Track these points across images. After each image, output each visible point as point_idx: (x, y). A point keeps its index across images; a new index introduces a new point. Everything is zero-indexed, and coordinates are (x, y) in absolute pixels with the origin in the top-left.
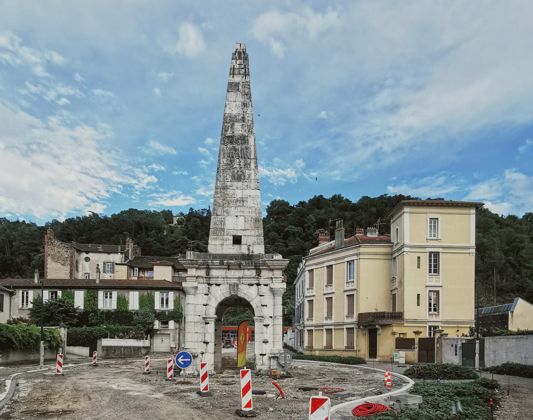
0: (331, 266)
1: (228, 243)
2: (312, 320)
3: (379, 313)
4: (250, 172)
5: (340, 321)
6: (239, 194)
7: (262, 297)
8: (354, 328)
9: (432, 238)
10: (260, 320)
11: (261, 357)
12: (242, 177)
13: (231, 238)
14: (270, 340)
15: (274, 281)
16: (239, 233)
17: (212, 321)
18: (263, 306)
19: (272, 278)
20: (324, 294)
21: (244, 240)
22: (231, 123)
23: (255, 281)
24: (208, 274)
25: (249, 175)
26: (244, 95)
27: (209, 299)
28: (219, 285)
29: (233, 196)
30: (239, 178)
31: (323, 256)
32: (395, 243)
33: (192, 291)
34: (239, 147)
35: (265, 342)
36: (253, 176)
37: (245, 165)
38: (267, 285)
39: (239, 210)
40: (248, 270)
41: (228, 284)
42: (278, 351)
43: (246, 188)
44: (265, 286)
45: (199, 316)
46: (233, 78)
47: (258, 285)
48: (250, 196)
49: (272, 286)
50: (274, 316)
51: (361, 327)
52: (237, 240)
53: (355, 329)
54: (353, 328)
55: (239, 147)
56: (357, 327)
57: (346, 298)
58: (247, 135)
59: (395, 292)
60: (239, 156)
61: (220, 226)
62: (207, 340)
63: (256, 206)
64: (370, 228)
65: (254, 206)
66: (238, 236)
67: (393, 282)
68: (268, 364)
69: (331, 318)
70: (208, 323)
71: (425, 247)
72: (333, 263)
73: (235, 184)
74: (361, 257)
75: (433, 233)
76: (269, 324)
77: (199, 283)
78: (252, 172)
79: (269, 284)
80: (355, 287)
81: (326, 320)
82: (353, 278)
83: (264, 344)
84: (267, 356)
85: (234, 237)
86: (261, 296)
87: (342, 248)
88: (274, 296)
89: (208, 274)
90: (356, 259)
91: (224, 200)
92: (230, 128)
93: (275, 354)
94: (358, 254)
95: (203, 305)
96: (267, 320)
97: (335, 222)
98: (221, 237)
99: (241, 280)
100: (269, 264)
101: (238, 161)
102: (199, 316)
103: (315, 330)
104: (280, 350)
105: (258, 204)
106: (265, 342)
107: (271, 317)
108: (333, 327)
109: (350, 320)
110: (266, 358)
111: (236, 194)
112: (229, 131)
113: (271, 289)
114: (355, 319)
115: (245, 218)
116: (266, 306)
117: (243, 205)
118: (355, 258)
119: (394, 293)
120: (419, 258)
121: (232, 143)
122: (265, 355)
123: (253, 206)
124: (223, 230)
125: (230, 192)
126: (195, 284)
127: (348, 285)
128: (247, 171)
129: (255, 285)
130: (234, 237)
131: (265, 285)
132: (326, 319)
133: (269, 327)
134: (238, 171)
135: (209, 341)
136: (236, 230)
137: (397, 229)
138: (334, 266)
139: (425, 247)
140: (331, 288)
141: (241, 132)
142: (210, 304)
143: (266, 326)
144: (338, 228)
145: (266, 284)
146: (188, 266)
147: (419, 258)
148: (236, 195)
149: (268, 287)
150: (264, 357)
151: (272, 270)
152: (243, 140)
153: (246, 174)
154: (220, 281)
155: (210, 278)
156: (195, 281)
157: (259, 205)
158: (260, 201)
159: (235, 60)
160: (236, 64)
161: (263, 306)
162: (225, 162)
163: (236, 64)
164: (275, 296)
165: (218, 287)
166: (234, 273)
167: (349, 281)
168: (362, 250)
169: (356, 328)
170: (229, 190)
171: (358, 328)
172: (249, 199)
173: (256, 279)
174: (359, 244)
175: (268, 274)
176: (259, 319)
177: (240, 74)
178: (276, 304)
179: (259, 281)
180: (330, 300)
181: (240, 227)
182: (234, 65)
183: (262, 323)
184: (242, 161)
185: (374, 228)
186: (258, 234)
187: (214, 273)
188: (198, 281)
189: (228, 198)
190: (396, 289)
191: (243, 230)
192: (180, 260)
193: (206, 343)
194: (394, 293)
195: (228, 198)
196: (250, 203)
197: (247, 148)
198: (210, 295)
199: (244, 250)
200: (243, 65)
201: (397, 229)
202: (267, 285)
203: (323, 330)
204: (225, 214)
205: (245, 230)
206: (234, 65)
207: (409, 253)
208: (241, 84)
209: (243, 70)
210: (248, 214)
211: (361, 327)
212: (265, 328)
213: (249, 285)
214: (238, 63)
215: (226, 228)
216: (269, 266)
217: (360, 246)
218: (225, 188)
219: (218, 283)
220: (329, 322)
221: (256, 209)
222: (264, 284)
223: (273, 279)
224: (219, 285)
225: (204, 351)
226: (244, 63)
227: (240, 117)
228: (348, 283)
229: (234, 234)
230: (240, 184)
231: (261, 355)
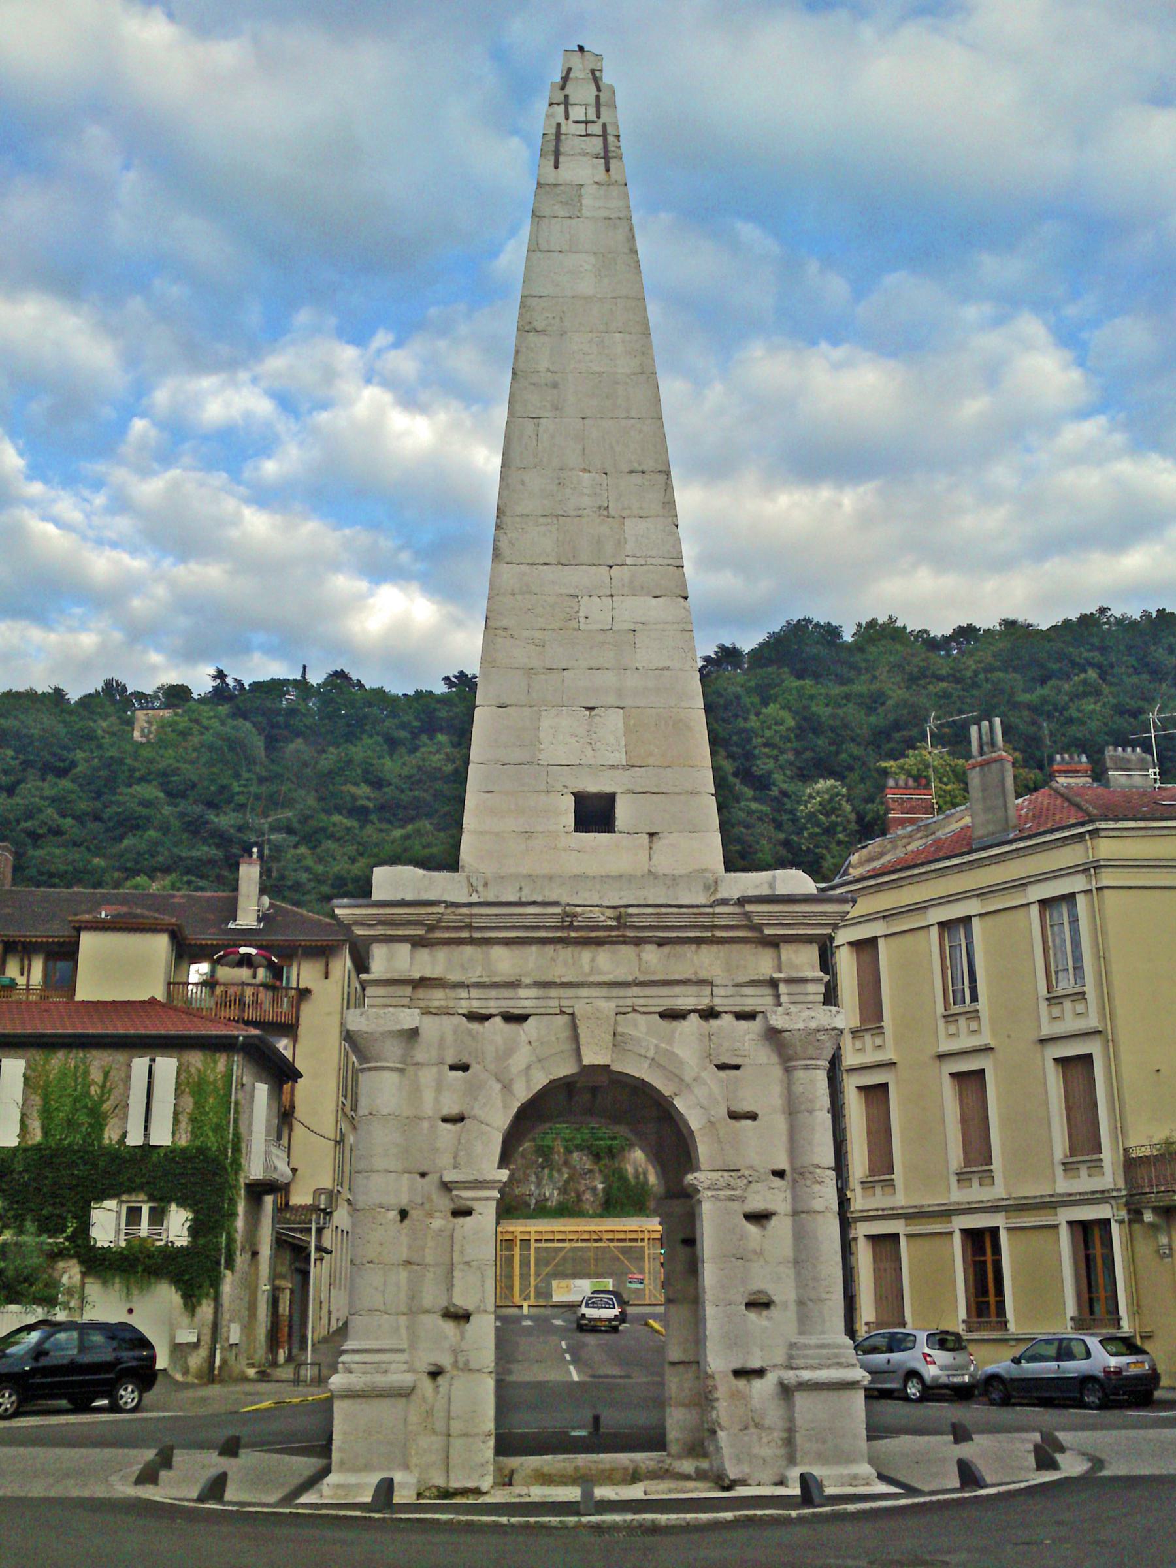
0: (872, 942)
2: (891, 1184)
5: (930, 1200)
8: (1109, 1220)
14: (784, 1292)
15: (784, 999)
17: (487, 1199)
18: (734, 1116)
19: (773, 984)
20: (941, 1057)
21: (623, 812)
27: (473, 1091)
28: (521, 1018)
31: (881, 896)
33: (392, 1051)
35: (760, 1304)
38: (750, 1016)
41: (562, 1013)
44: (743, 1022)
45: (423, 1175)
46: (556, 167)
49: (777, 1020)
50: (794, 1169)
51: (1148, 1217)
53: (1115, 1227)
54: (1107, 1222)
56: (1123, 1214)
57: (948, 1090)
62: (461, 1301)
64: (1129, 749)
68: (781, 1424)
69: (987, 1177)
70: (468, 1212)
72: (971, 907)
74: (1107, 878)
76: (771, 1207)
77: (426, 1012)
79: (758, 1009)
80: (1093, 1022)
81: (1070, 1174)
82: (974, 998)
83: (752, 1316)
84: (771, 1378)
85: (581, 799)
86: (722, 1067)
87: (1011, 842)
88: (788, 1070)
90: (1085, 892)
94: (1091, 868)
95: (445, 1120)
97: (964, 727)
102: (423, 1175)
103: (907, 1236)
106: (760, 1304)
107: (780, 1174)
108: (997, 1220)
109: (1085, 1183)
110: (763, 1389)
111: (581, 614)
113: (773, 1035)
114: (1110, 1177)
115: (626, 718)
118: (1077, 884)
122: (760, 1373)
123: (661, 666)
126: (409, 1018)
127: (1056, 1011)
129: (694, 1017)
130: (581, 799)
131: (740, 1016)
132: (963, 1177)
133: (774, 1221)
135: (471, 1308)
138: (881, 942)
142: (477, 1111)
144: (981, 753)
145: (747, 1009)
146: (379, 931)
148: (582, 620)
149: (756, 1026)
150: (758, 1384)
151: (774, 943)
154: (525, 999)
156: (406, 1001)
159: (562, 107)
160: (567, 118)
161: (734, 1116)
163: (567, 118)
164: (795, 1068)
165: (513, 1027)
166: (593, 960)
167: (955, 1009)
168: (1106, 848)
169: (1121, 1222)
171: (1130, 1222)
174: (1091, 821)
178: (803, 1107)
180: (970, 1082)
182: (559, 125)
185: (1133, 751)
188: (422, 1004)
192: (338, 907)
193: (461, 1317)
200: (593, 122)
202: (750, 1016)
203: (1056, 1226)
206: (559, 125)
211: (1148, 1217)
212: (752, 1229)
213: (663, 1015)
216: (758, 928)
217: (1097, 830)
219: (517, 1009)
220: (977, 1193)
222: (737, 1009)
223: (783, 988)
224: (521, 1018)
225: (446, 1361)
226: (599, 117)
228: (1054, 1000)
231: (739, 1373)
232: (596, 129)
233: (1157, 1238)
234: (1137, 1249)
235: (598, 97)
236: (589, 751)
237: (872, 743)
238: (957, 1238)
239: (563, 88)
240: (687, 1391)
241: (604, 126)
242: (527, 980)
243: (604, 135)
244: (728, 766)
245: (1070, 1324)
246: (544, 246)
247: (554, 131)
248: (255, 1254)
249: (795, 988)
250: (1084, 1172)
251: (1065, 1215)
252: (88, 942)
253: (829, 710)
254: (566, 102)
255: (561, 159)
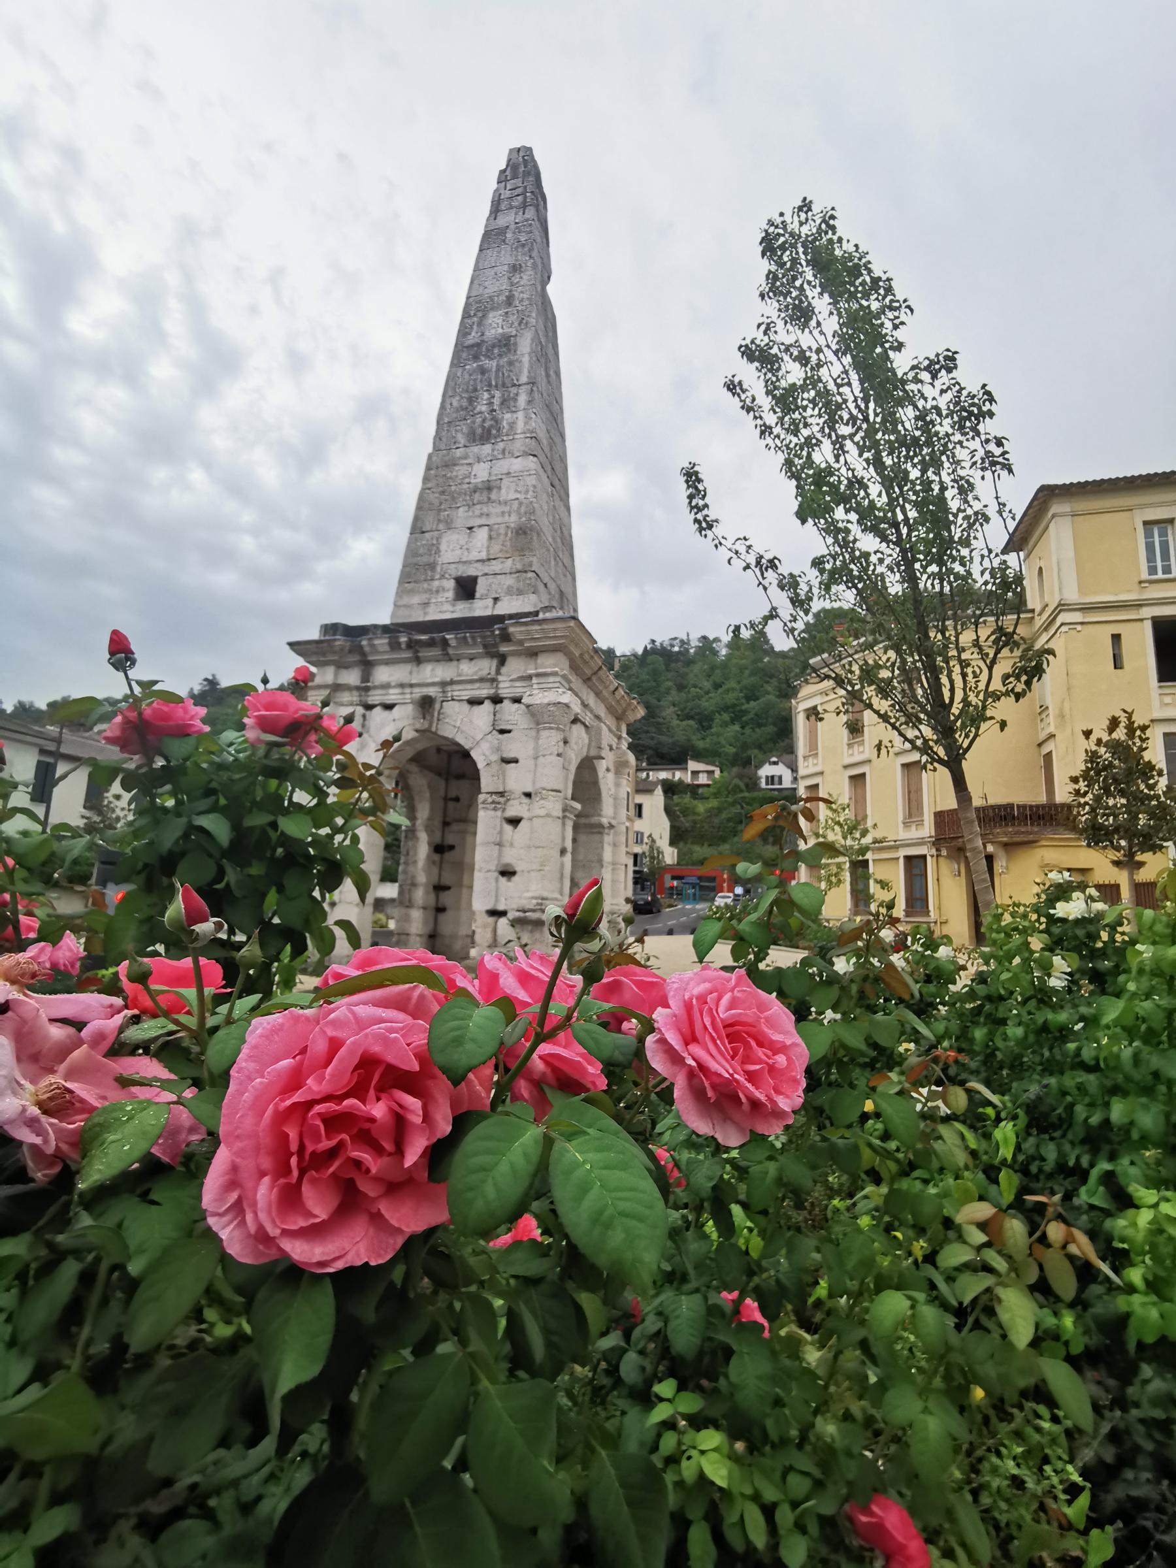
1: (440, 600)
3: (993, 807)
4: (515, 415)
6: (481, 473)
7: (506, 735)
9: (1160, 575)
10: (493, 802)
11: (491, 920)
12: (494, 432)
13: (450, 584)
16: (471, 571)
20: (846, 767)
21: (480, 589)
22: (480, 314)
23: (484, 691)
24: (366, 677)
25: (512, 425)
26: (516, 248)
29: (467, 480)
30: (486, 435)
32: (1038, 610)
34: (492, 364)
35: (507, 873)
36: (520, 426)
37: (502, 403)
39: (477, 512)
40: (471, 659)
42: (534, 901)
43: (500, 456)
47: (497, 700)
48: (509, 473)
52: (466, 588)
53: (929, 858)
54: (924, 857)
55: (492, 364)
56: (934, 852)
58: (514, 333)
59: (1049, 747)
60: (490, 385)
61: (425, 559)
63: (521, 496)
65: (518, 496)
66: (469, 577)
67: (1042, 720)
71: (1138, 605)
73: (475, 449)
75: (1159, 564)
78: (520, 415)
83: (503, 880)
86: (502, 732)
89: (366, 677)
91: (443, 493)
92: (475, 327)
93: (525, 912)
96: (515, 802)
98: (426, 586)
99: (449, 688)
100: (519, 637)
101: (486, 395)
104: (543, 899)
105: (527, 492)
106: (507, 873)
109: (914, 833)
112: (473, 334)
114: (928, 829)
115: (490, 530)
116: (516, 761)
117: (489, 499)
119: (1046, 749)
120: (1116, 638)
121: (476, 358)
124: (432, 566)
125: (460, 473)
128: (508, 416)
129: (487, 702)
134: (484, 421)
136: (465, 562)
137: (1040, 569)
139: (1138, 605)
140: (861, 749)
141: (500, 331)
143: (515, 822)
147: (1116, 638)
151: (533, 654)
152: (505, 345)
153: (505, 423)
154: (393, 696)
155: (367, 689)
157: (531, 493)
158: (534, 482)
162: (455, 404)
165: (387, 713)
169: (932, 856)
170: (457, 468)
172: (505, 483)
173: (488, 685)
175: (523, 668)
176: (490, 800)
177: (511, 208)
179: (497, 688)
181: (474, 555)
183: (499, 813)
184: (498, 394)
186: (519, 567)
187: (382, 674)
189: (453, 488)
190: (1052, 736)
191: (482, 561)
194: (1046, 749)
195: (453, 488)
196: (507, 492)
197: (511, 363)
198: (365, 735)
199: (480, 608)
201: (1040, 569)
204: (441, 526)
205: (489, 560)
207: (1079, 627)
208: (513, 226)
209: (520, 198)
210: (499, 520)
214: (509, 187)
215: (440, 560)
218: (450, 464)
221: (521, 504)
227: (503, 298)
229: (459, 574)
230: (487, 449)
234: (443, 873)
236: (466, 553)
237: (1113, 747)
238: (901, 861)
242: (393, 684)
244: (567, 561)
249: (542, 680)
250: (914, 827)
251: (902, 853)
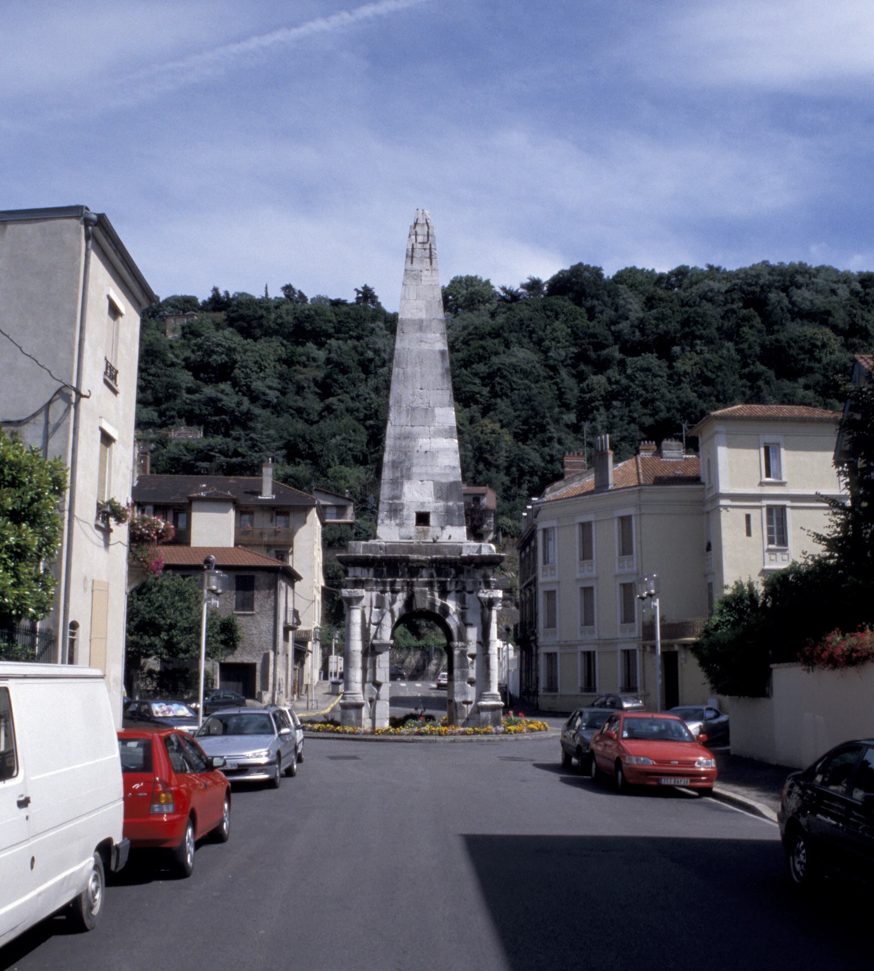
53: (638, 652)
182: (413, 245)
206: (413, 245)
232: (427, 246)
233: (183, 696)
235: (428, 232)
238: (579, 654)
239: (415, 228)
240: (683, 369)
241: (430, 245)
243: (430, 249)
245: (619, 690)
246: (407, 298)
247: (411, 247)
248: (287, 655)
252: (232, 545)
253: (530, 365)
254: (416, 234)
255: (414, 259)
